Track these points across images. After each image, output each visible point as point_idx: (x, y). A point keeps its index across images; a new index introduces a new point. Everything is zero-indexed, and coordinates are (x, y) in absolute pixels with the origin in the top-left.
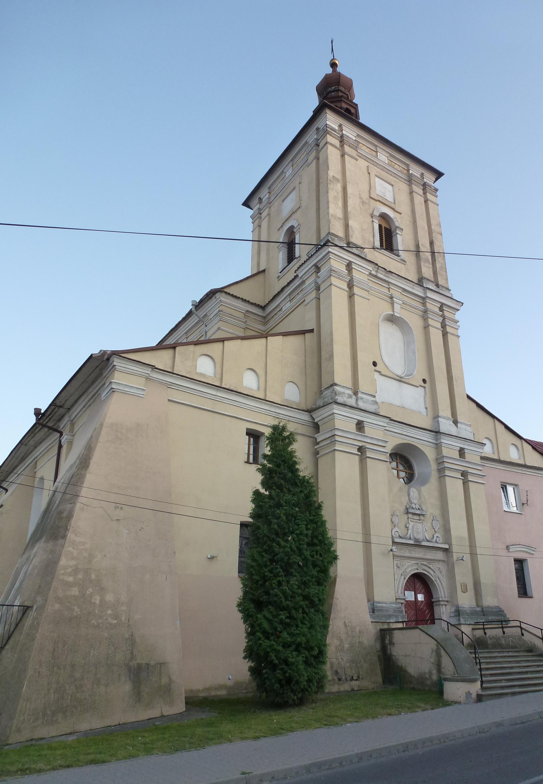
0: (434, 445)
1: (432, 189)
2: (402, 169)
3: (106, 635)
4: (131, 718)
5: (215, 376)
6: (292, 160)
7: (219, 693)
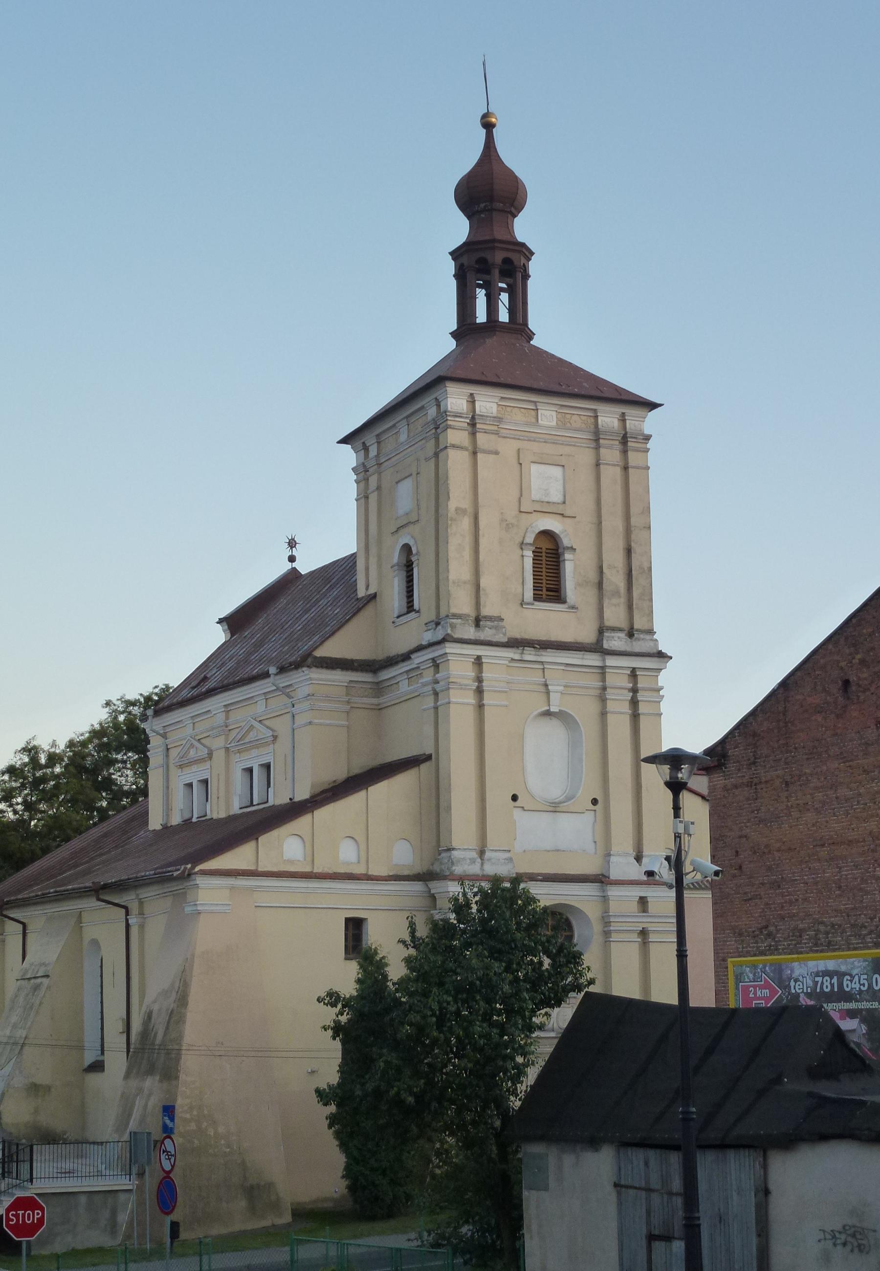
0: (598, 897)
1: (640, 439)
2: (585, 417)
3: (222, 1161)
4: (250, 1226)
5: (305, 860)
6: (407, 417)
7: (325, 1205)
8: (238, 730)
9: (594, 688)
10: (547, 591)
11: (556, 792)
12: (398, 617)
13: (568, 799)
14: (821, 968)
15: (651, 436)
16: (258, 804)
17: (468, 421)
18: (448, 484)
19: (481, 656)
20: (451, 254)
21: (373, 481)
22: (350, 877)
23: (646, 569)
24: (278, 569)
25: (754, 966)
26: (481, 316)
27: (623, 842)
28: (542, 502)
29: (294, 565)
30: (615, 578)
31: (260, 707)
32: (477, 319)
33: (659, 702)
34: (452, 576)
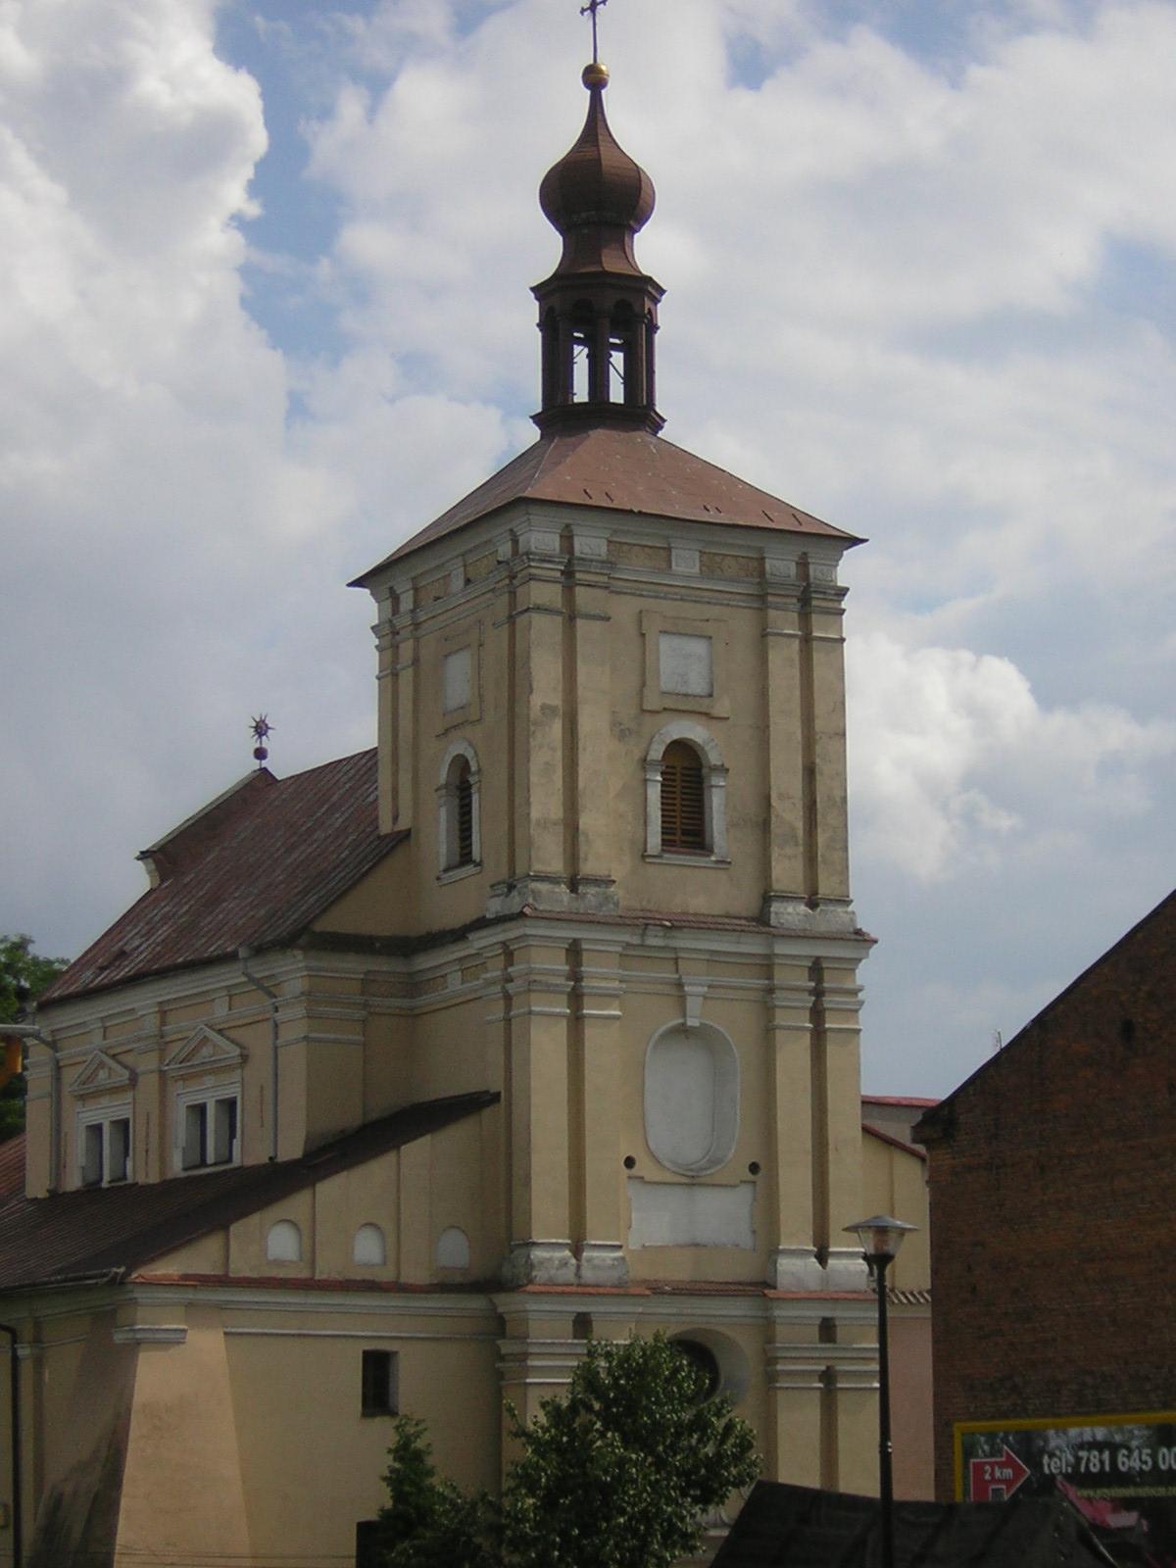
8: (180, 1044)
9: (757, 989)
10: (683, 834)
11: (693, 1152)
12: (446, 871)
13: (713, 1163)
14: (1087, 1437)
15: (848, 589)
16: (215, 1164)
17: (562, 568)
18: (529, 668)
19: (580, 939)
20: (533, 289)
21: (406, 649)
22: (370, 1287)
23: (838, 799)
24: (231, 770)
25: (991, 1436)
26: (581, 393)
27: (796, 1233)
28: (678, 694)
29: (265, 764)
30: (788, 813)
31: (220, 1010)
32: (575, 397)
33: (857, 1011)
34: (535, 813)
